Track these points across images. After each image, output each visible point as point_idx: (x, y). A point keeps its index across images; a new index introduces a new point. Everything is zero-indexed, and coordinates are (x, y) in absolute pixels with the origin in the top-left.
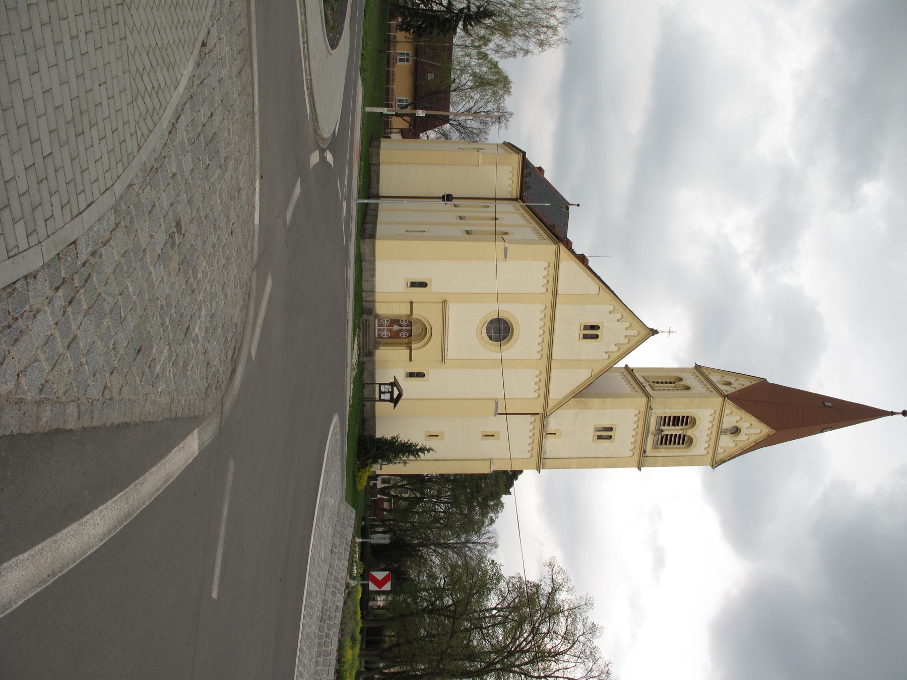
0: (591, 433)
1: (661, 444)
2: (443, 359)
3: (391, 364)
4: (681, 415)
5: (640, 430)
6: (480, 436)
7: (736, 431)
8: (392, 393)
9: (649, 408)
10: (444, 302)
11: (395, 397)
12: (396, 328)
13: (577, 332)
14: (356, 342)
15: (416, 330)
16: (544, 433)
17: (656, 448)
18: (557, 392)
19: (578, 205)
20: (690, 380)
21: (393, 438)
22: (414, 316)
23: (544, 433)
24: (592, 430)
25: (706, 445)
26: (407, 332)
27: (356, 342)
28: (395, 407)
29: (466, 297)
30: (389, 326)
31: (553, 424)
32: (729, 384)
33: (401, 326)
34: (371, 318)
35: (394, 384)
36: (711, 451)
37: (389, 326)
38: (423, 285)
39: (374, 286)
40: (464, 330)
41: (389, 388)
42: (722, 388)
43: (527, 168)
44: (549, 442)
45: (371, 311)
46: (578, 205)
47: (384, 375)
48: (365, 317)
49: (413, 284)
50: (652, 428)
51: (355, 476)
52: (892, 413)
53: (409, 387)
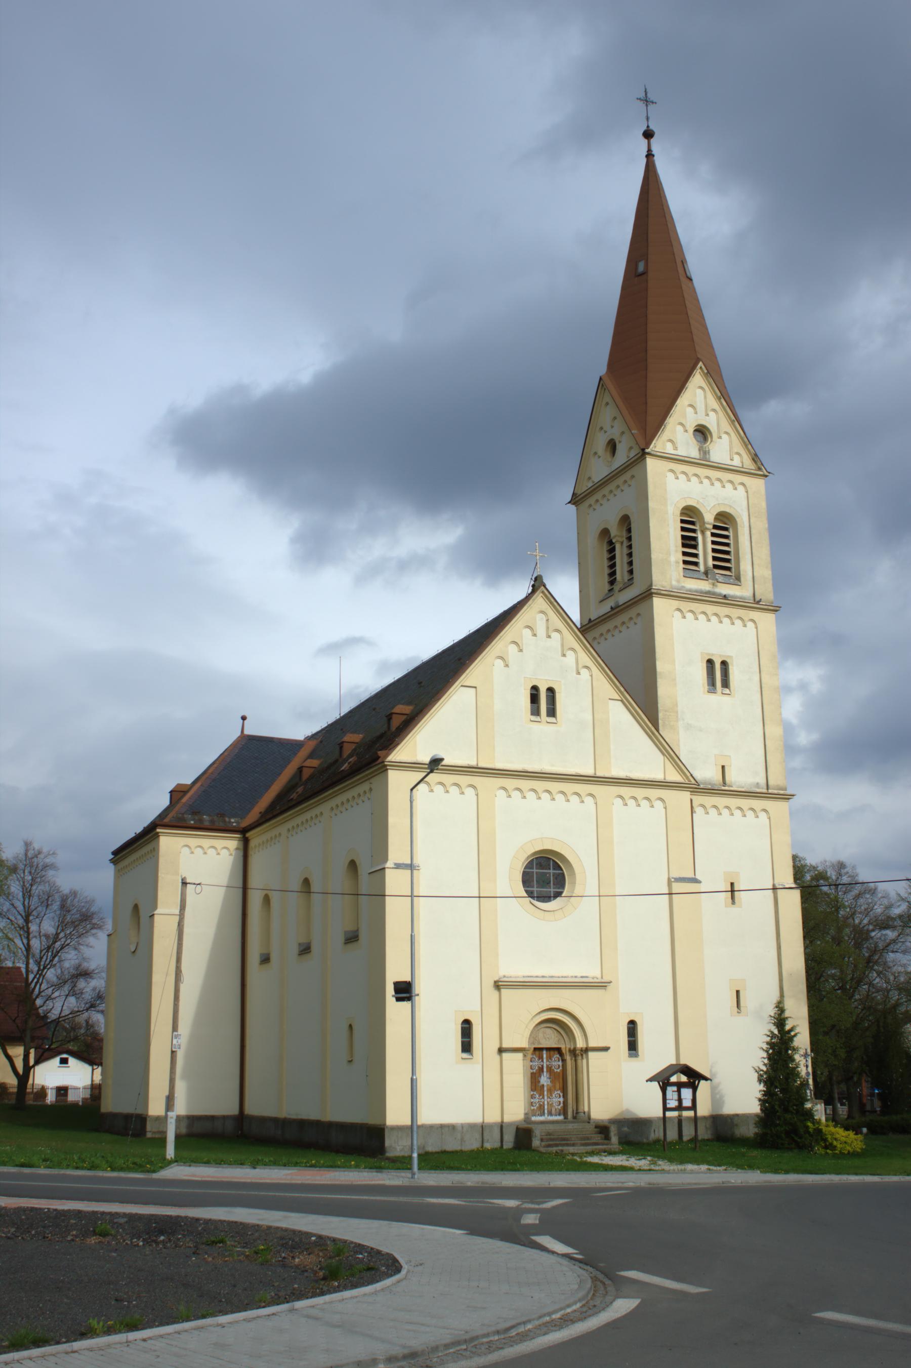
0: (718, 699)
1: (728, 569)
2: (602, 985)
3: (621, 1088)
4: (680, 533)
5: (710, 609)
6: (734, 910)
7: (702, 432)
8: (680, 1085)
9: (668, 595)
10: (498, 986)
11: (684, 1079)
12: (544, 1080)
13: (543, 728)
14: (595, 1159)
15: (550, 1039)
16: (721, 789)
17: (738, 578)
18: (654, 766)
19: (244, 718)
20: (607, 514)
21: (760, 1081)
22: (524, 1044)
23: (721, 789)
24: (712, 696)
25: (729, 486)
26: (557, 1057)
27: (595, 1159)
28: (706, 1079)
29: (486, 946)
30: (541, 1094)
31: (706, 773)
32: (612, 446)
33: (541, 1069)
34: (538, 1132)
35: (663, 1080)
36: (738, 478)
37: (541, 1094)
38: (467, 1028)
39: (472, 1126)
40: (547, 944)
41: (671, 1090)
42: (622, 457)
43: (182, 819)
44: (739, 778)
45: (523, 1135)
46: (244, 718)
47: (647, 1103)
48: (536, 1143)
49: (467, 1047)
50: (704, 585)
51: (842, 1155)
52: (650, 155)
53: (658, 1054)
